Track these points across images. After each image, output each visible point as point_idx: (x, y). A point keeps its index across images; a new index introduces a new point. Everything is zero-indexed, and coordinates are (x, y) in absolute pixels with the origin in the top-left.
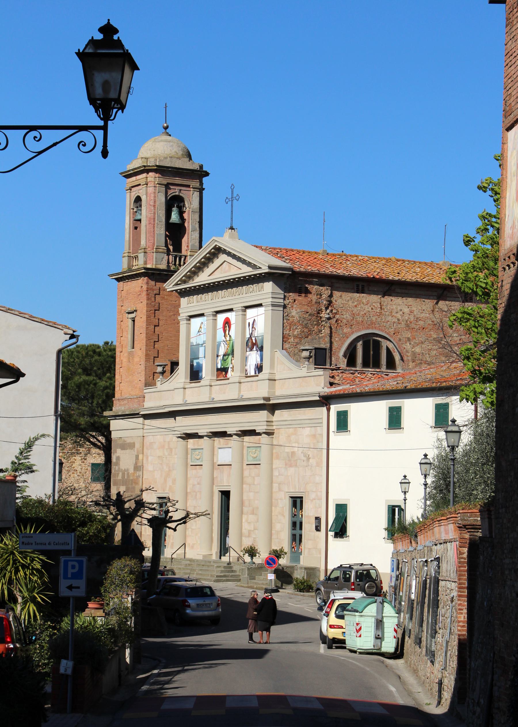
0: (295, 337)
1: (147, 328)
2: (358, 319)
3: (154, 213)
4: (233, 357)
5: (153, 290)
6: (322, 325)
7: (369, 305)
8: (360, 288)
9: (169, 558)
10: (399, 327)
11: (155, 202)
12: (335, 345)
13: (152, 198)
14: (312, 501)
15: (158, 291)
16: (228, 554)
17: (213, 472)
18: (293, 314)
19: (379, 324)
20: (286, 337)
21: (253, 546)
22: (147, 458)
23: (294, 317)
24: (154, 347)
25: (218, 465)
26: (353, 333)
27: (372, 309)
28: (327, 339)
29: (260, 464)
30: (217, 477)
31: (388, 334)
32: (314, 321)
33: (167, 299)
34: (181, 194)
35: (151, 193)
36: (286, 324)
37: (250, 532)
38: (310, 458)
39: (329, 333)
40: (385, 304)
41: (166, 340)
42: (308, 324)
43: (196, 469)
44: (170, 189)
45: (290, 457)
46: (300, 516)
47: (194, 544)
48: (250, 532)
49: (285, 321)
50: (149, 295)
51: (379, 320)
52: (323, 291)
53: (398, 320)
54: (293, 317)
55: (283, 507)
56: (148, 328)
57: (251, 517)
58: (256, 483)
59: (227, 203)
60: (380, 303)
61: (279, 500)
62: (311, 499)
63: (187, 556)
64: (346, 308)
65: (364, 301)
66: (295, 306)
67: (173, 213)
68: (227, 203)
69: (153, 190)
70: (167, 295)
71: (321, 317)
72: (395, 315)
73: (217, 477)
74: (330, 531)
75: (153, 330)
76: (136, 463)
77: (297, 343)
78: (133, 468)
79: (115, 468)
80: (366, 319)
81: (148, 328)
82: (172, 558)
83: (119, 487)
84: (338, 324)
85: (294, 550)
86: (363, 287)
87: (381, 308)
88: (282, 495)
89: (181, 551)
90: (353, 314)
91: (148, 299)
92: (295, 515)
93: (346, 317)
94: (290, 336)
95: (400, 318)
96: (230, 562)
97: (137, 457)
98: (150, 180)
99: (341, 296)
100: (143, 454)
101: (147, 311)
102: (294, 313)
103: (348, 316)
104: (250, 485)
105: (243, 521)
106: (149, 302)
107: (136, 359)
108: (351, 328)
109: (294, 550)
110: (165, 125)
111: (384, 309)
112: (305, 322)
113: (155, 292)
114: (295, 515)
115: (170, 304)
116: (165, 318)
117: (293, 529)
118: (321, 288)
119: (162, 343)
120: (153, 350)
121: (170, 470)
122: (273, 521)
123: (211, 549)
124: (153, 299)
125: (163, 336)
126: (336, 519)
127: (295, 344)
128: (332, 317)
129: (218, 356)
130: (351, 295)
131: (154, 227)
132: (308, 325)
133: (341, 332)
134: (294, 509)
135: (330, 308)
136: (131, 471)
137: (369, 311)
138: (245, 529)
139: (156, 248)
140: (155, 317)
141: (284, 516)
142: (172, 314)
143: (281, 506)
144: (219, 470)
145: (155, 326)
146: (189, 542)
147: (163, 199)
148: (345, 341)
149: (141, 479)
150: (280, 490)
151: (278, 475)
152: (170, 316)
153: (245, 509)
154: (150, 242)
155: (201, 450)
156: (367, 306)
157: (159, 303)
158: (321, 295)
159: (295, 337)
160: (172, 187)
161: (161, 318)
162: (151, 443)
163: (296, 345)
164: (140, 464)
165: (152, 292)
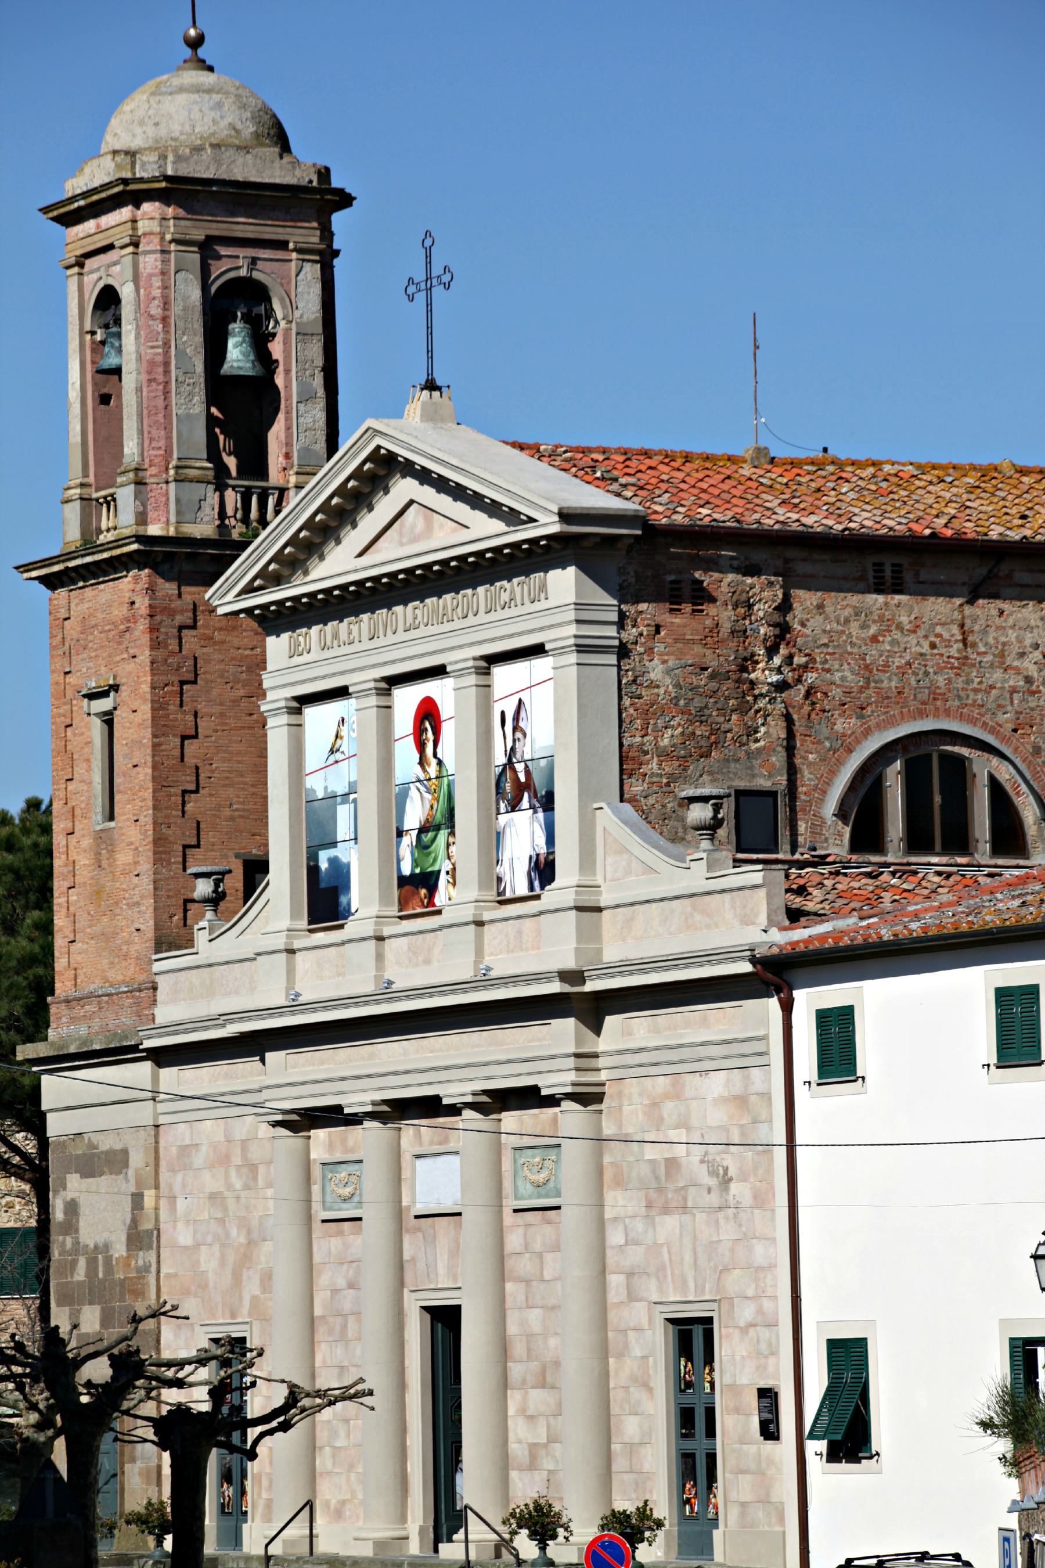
0: (664, 755)
1: (155, 746)
2: (885, 684)
3: (166, 344)
4: (452, 833)
5: (172, 613)
6: (757, 711)
7: (921, 633)
8: (888, 573)
9: (258, 1557)
10: (1033, 704)
11: (166, 305)
12: (807, 777)
13: (157, 293)
14: (744, 1330)
15: (191, 614)
16: (460, 1536)
17: (401, 1241)
18: (652, 676)
19: (959, 697)
20: (633, 759)
21: (542, 1502)
22: (173, 1199)
23: (658, 687)
24: (183, 812)
25: (417, 1217)
26: (867, 733)
27: (933, 646)
28: (778, 759)
29: (558, 1208)
30: (413, 1260)
31: (992, 731)
32: (728, 698)
33: (223, 642)
34: (256, 275)
35: (151, 275)
36: (631, 711)
37: (533, 1448)
38: (731, 1179)
39: (783, 735)
40: (976, 628)
41: (225, 786)
42: (706, 706)
43: (340, 1234)
44: (219, 257)
45: (663, 1178)
46: (707, 1385)
47: (343, 1503)
48: (533, 1448)
49: (627, 702)
50: (158, 630)
51: (959, 683)
52: (757, 590)
53: (1029, 680)
54: (653, 685)
55: (644, 1358)
56: (159, 744)
57: (538, 1398)
58: (547, 1276)
59: (411, 298)
60: (962, 626)
61: (630, 1334)
62: (742, 1324)
63: (323, 1547)
64: (838, 646)
65: (904, 619)
66: (659, 648)
67: (231, 342)
68: (411, 298)
69: (159, 263)
70: (221, 629)
71: (753, 684)
72: (1016, 663)
73: (413, 1260)
74: (812, 1436)
75: (177, 753)
76: (135, 1222)
77: (672, 778)
78: (124, 1238)
79: (64, 1242)
80: (913, 683)
81: (159, 744)
82: (268, 1558)
83: (79, 1311)
84: (813, 703)
85: (692, 1509)
86: (897, 569)
87: (964, 641)
88: (638, 1313)
89: (298, 1530)
90: (867, 667)
91: (156, 645)
92: (689, 1385)
93: (843, 679)
94: (646, 753)
95: (1035, 675)
96: (468, 1562)
97: (137, 1199)
98: (147, 230)
99: (820, 607)
100: (157, 1187)
101: (153, 688)
102: (656, 671)
103: (847, 674)
104: (528, 1282)
105: (511, 1411)
106: (160, 654)
107: (124, 858)
108: (860, 717)
109: (692, 1509)
110: (192, 32)
111: (974, 645)
112: (698, 702)
113: (179, 619)
114: (689, 1385)
115: (233, 659)
116: (217, 709)
117: (684, 1436)
118: (749, 580)
119: (211, 795)
120: (180, 821)
121: (251, 1243)
122: (615, 1409)
123: (403, 1518)
124: (173, 645)
125: (213, 772)
126: (830, 1394)
127: (665, 781)
128: (790, 681)
129: (400, 834)
130: (854, 599)
131: (166, 393)
132: (707, 712)
133: (826, 732)
134: (683, 1363)
135: (783, 651)
136: (119, 1250)
137: (921, 654)
138: (519, 1442)
139: (177, 467)
140: (181, 706)
141: (650, 1390)
142: (242, 692)
143: (639, 1355)
144: (420, 1235)
145: (184, 738)
146: (327, 1493)
147: (195, 294)
148: (840, 763)
149: (152, 1279)
150: (632, 1296)
151: (622, 1242)
152: (234, 701)
153: (516, 1370)
154: (154, 444)
155: (357, 1166)
156: (913, 636)
157: (195, 658)
158: (750, 606)
159: (664, 755)
160: (223, 251)
161: (202, 708)
162: (185, 1150)
163: (668, 784)
164: (147, 1225)
165: (168, 621)
